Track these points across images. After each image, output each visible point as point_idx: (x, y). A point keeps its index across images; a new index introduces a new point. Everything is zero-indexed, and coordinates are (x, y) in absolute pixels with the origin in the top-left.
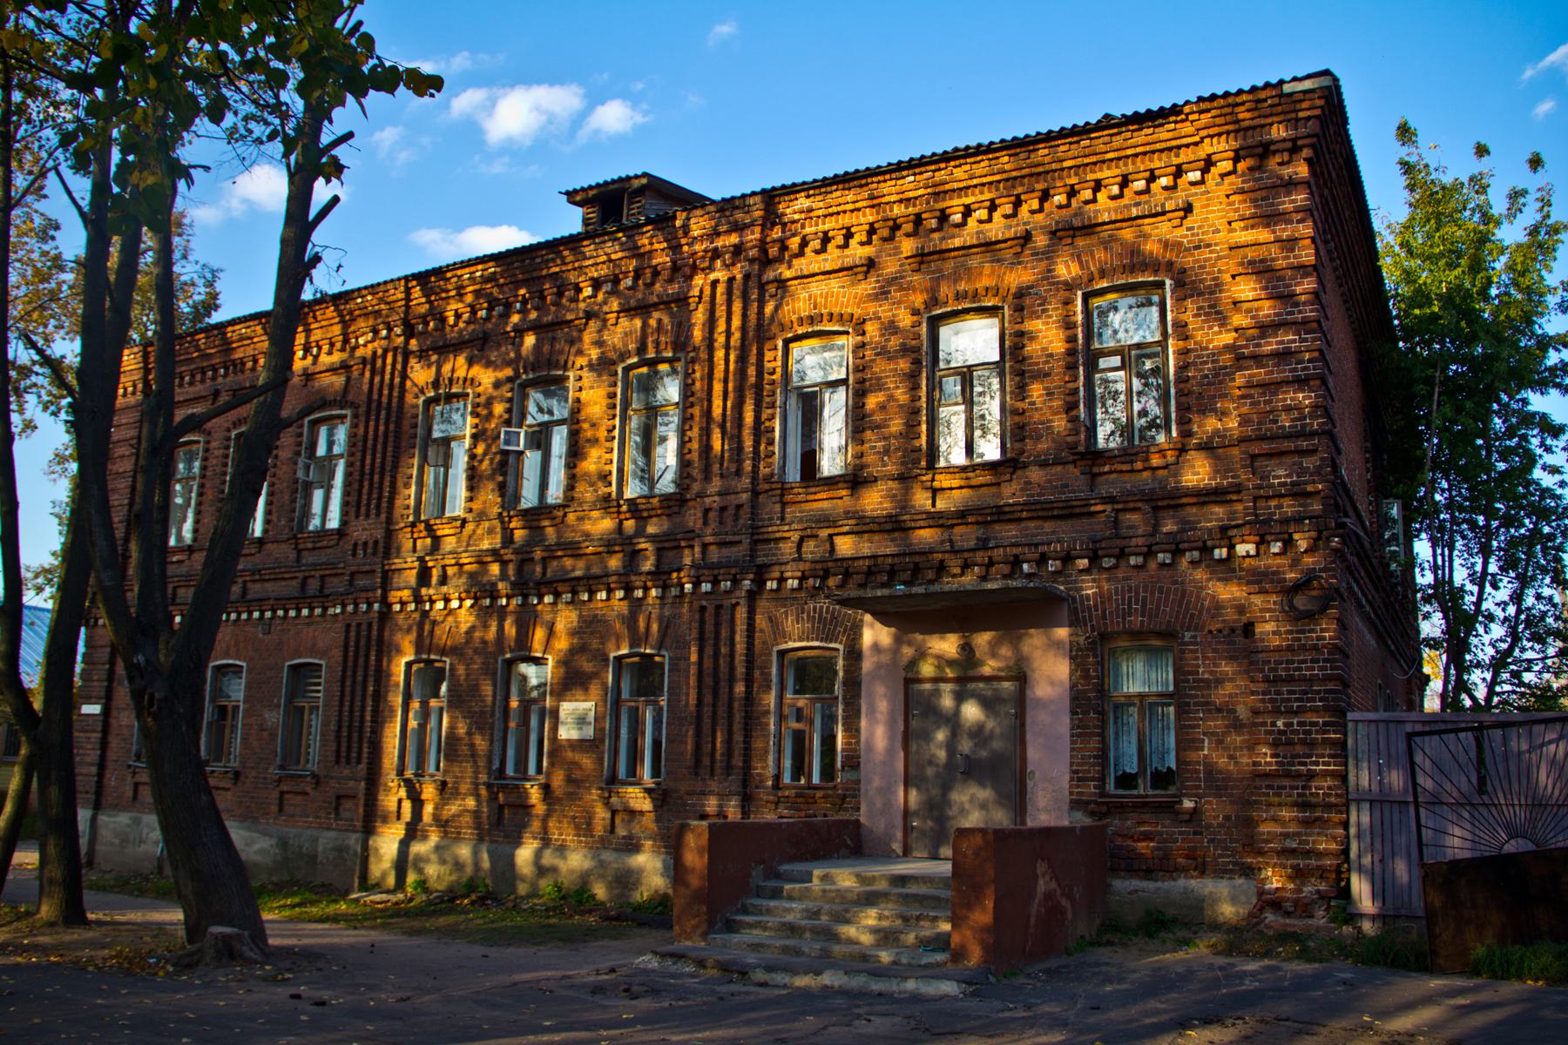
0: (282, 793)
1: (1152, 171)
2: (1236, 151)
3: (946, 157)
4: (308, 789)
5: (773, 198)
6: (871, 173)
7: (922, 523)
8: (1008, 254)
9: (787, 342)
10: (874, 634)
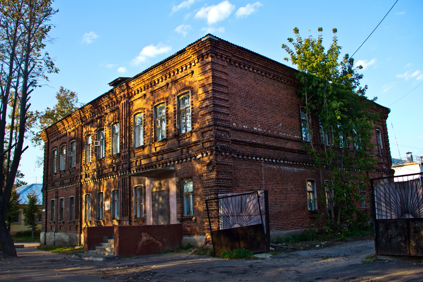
0: (70, 226)
1: (186, 64)
2: (197, 57)
5: (127, 83)
8: (165, 89)
9: (135, 116)
10: (147, 182)
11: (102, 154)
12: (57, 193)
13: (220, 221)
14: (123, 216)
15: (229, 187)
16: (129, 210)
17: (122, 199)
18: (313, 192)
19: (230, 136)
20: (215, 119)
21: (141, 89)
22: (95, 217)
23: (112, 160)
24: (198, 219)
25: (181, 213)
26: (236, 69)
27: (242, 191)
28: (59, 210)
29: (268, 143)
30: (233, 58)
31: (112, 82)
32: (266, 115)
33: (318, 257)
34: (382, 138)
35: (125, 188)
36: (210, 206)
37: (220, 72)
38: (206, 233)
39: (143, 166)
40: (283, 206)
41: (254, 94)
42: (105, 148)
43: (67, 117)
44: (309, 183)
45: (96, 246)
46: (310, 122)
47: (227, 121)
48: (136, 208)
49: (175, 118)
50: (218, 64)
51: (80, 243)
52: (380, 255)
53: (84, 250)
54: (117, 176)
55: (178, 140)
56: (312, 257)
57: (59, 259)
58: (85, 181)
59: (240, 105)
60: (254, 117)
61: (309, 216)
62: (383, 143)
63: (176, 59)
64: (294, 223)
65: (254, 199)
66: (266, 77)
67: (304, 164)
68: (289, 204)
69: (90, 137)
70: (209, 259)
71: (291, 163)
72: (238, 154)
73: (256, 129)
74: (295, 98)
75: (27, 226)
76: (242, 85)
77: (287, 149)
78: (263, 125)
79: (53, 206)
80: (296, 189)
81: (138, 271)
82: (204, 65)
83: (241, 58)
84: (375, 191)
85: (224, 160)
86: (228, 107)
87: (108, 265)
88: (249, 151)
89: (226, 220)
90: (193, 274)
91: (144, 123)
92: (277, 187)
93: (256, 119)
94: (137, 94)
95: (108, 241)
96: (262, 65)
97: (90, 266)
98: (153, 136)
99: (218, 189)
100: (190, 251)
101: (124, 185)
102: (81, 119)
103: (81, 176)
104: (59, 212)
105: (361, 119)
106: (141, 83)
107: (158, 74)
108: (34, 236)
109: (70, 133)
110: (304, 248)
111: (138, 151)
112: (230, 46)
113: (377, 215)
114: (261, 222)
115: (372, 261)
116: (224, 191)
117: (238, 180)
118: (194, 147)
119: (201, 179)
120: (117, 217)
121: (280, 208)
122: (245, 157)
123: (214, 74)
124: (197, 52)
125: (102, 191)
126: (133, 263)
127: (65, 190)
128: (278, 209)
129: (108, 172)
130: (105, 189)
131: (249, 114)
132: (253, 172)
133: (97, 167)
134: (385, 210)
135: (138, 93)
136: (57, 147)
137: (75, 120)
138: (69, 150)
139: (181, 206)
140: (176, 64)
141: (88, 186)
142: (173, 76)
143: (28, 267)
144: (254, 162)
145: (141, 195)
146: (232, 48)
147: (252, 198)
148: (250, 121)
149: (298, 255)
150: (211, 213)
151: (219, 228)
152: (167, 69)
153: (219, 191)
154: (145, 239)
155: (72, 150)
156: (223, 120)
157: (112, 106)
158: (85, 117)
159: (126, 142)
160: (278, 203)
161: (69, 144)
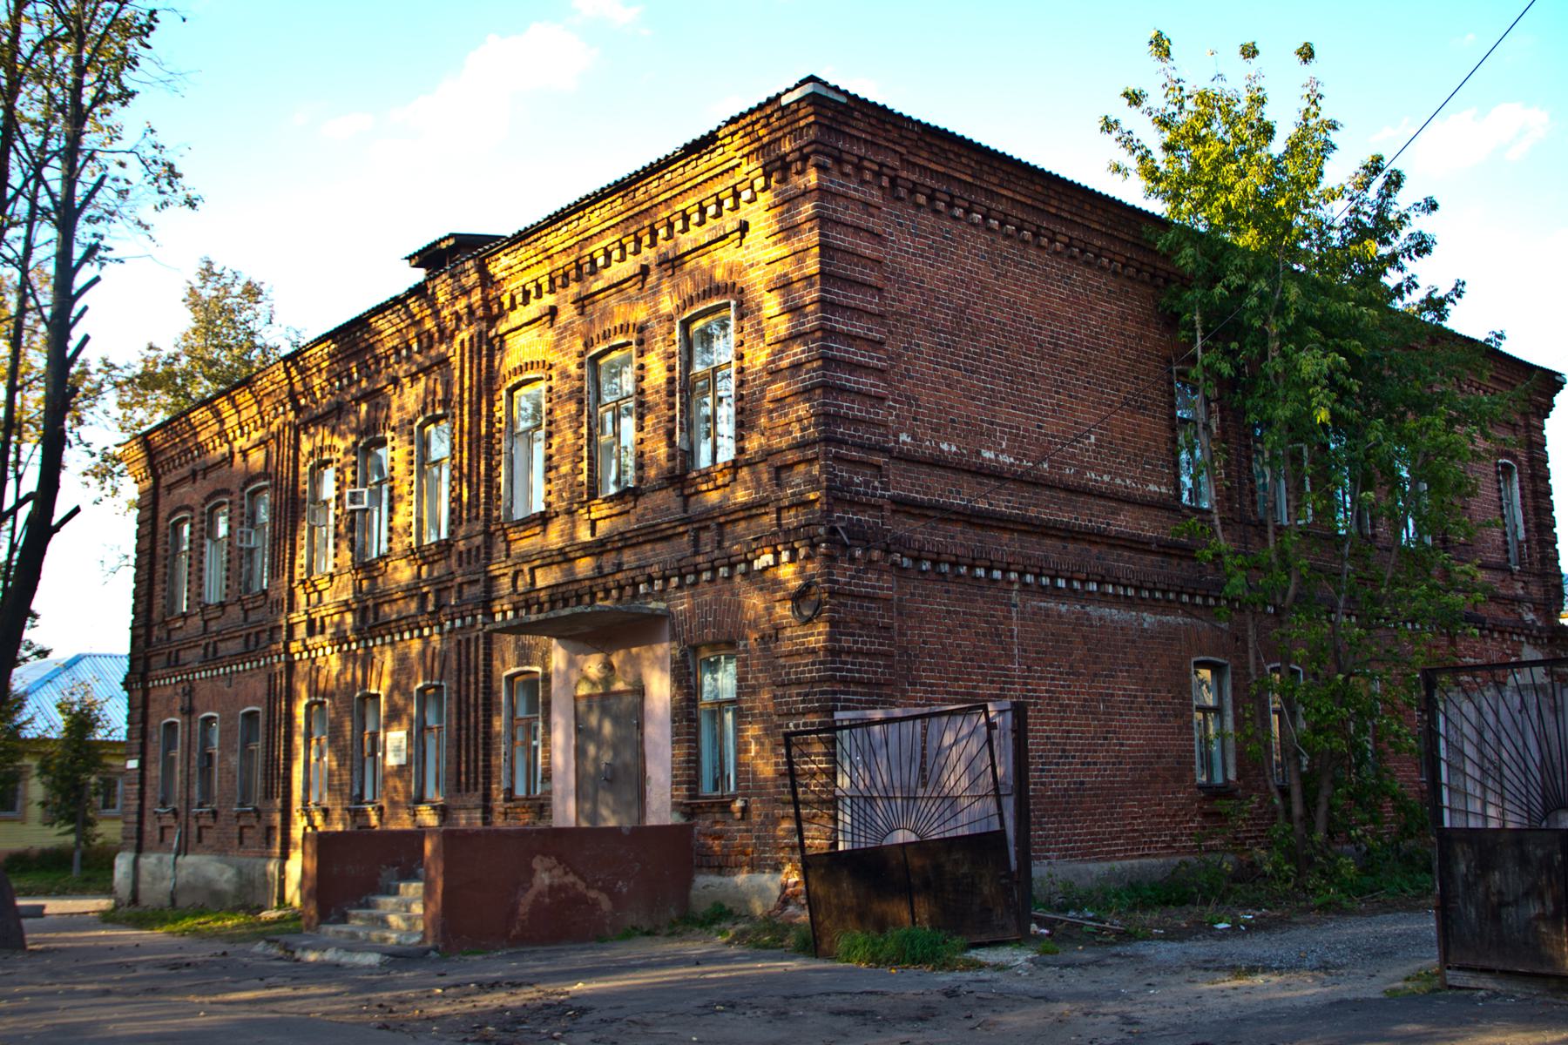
0: (242, 828)
1: (717, 194)
3: (579, 207)
4: (255, 824)
5: (484, 259)
6: (537, 229)
7: (578, 554)
8: (633, 291)
9: (511, 392)
10: (558, 657)
11: (378, 544)
12: (190, 693)
13: (840, 816)
14: (459, 791)
15: (878, 684)
16: (484, 766)
17: (454, 722)
18: (1218, 710)
19: (888, 483)
20: (826, 418)
21: (539, 287)
22: (348, 791)
23: (419, 568)
24: (756, 806)
25: (689, 783)
26: (916, 216)
27: (928, 699)
29: (1039, 513)
30: (904, 174)
31: (415, 254)
32: (1032, 400)
33: (1217, 969)
34: (1522, 497)
36: (800, 756)
37: (851, 230)
38: (783, 865)
39: (542, 594)
40: (1095, 764)
41: (985, 319)
42: (391, 519)
43: (237, 382)
44: (1206, 674)
45: (352, 908)
46: (1215, 430)
48: (512, 759)
49: (672, 407)
50: (846, 197)
51: (282, 897)
52: (1459, 969)
53: (303, 923)
54: (436, 629)
55: (682, 495)
56: (1193, 967)
57: (199, 957)
58: (306, 648)
60: (983, 408)
61: (1200, 808)
62: (1524, 515)
63: (681, 170)
64: (1137, 831)
65: (970, 735)
66: (1040, 247)
67: (1185, 598)
68: (1117, 757)
69: (330, 474)
70: (794, 965)
71: (1131, 592)
72: (916, 553)
73: (993, 456)
75: (55, 830)
77: (1114, 538)
78: (1017, 441)
79: (170, 744)
80: (1147, 697)
81: (518, 1004)
82: (788, 202)
83: (937, 172)
84: (1441, 719)
85: (860, 578)
86: (882, 371)
87: (400, 982)
88: (962, 545)
89: (862, 813)
90: (728, 1016)
91: (550, 423)
92: (1069, 686)
93: (994, 417)
94: (520, 307)
95: (397, 888)
96: (1023, 199)
97: (328, 984)
98: (584, 477)
99: (835, 692)
100: (722, 932)
101: (464, 668)
102: (293, 396)
103: (291, 628)
104: (195, 770)
105: (1428, 418)
106: (538, 263)
107: (608, 228)
108: (83, 868)
109: (245, 453)
110: (1166, 933)
111: (523, 534)
112: (894, 125)
113: (1446, 813)
114: (996, 827)
115: (1424, 987)
116: (859, 701)
117: (916, 656)
118: (743, 524)
119: (769, 649)
121: (1080, 770)
122: (945, 568)
123: (827, 236)
124: (763, 147)
125: (374, 691)
126: (499, 974)
127: (223, 684)
128: (1072, 777)
129: (399, 612)
130: (386, 682)
131: (965, 396)
132: (975, 627)
133: (354, 593)
134: (1478, 793)
135: (526, 302)
136: (189, 508)
137: (266, 402)
138: (242, 523)
139: (689, 754)
140: (680, 194)
141: (318, 670)
142: (666, 239)
144: (981, 588)
145: (532, 707)
147: (965, 731)
148: (967, 424)
149: (1141, 958)
150: (807, 786)
151: (835, 844)
152: (641, 212)
153: (839, 700)
154: (547, 881)
155: (253, 525)
156: (861, 421)
157: (419, 352)
158: (309, 391)
159: (474, 497)
160: (1076, 751)
161: (242, 498)
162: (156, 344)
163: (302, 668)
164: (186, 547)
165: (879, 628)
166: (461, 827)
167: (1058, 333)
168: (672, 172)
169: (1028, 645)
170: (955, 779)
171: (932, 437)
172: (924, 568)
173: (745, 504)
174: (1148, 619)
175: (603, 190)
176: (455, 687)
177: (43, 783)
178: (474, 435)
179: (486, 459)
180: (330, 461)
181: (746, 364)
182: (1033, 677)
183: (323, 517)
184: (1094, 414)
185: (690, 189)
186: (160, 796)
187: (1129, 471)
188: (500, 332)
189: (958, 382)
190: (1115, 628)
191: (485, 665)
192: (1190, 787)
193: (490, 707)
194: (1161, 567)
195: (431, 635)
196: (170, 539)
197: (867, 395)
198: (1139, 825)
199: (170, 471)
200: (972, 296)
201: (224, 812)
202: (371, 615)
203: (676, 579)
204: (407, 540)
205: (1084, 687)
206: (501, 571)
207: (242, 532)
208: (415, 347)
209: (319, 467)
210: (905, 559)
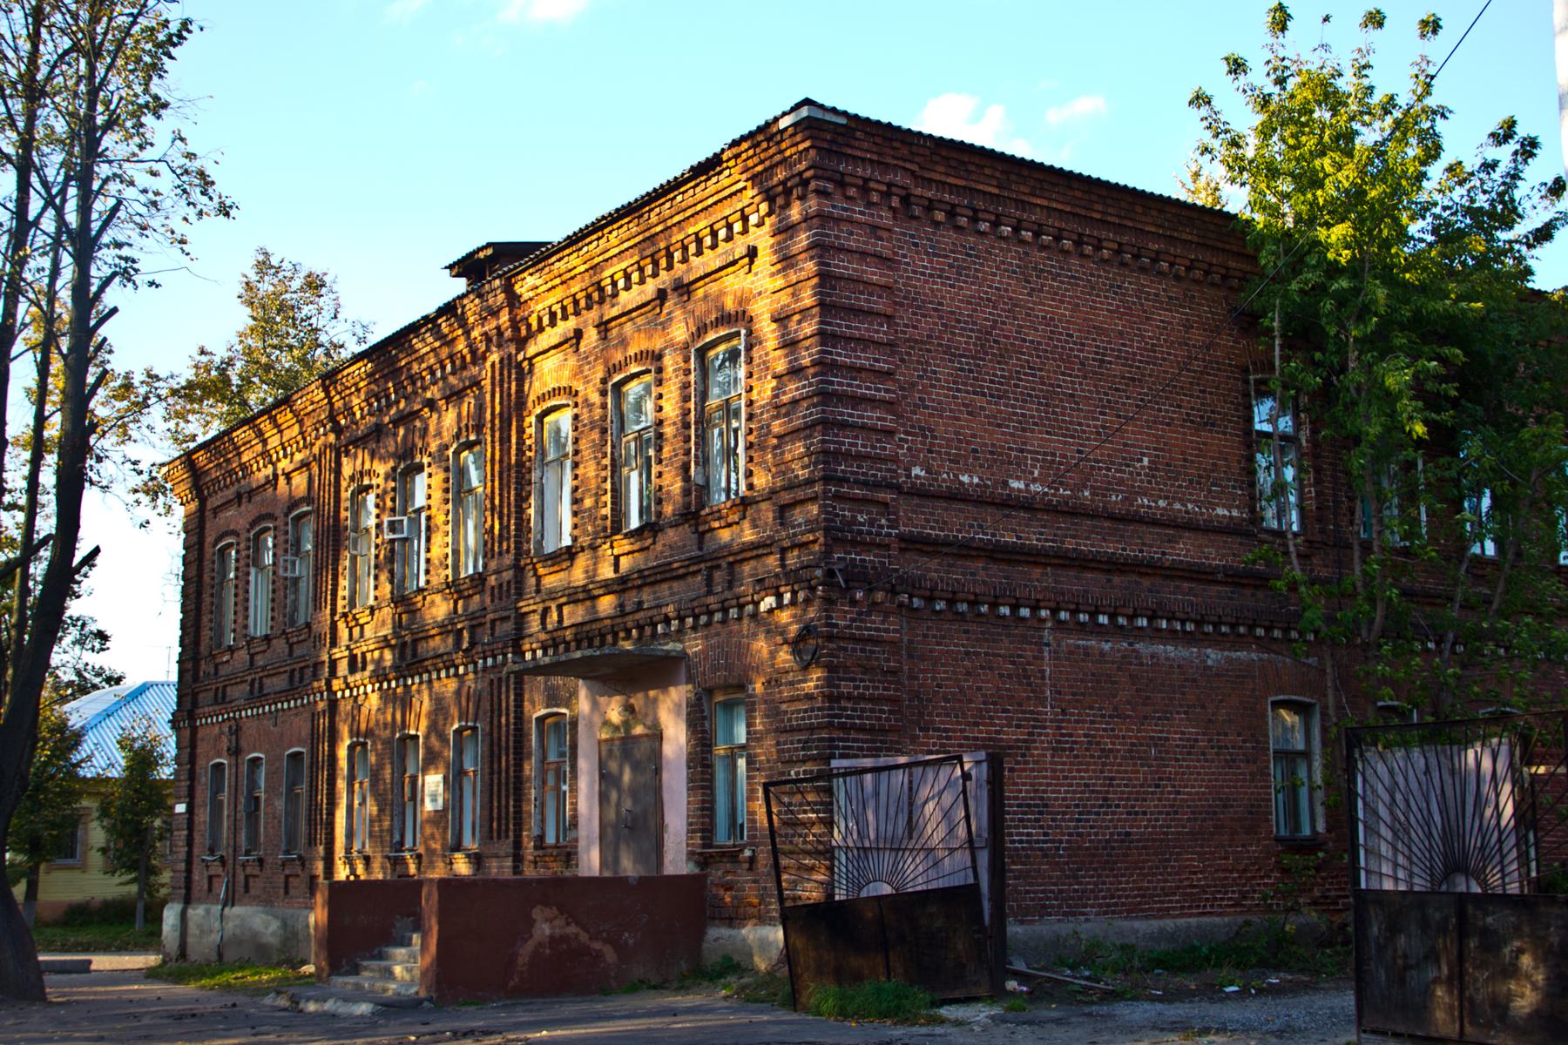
0: (287, 877)
1: (726, 218)
7: (601, 591)
9: (540, 418)
12: (236, 731)
15: (882, 731)
16: (515, 812)
19: (896, 521)
20: (826, 457)
25: (703, 831)
28: (241, 807)
30: (918, 191)
31: (455, 263)
32: (1071, 422)
35: (500, 721)
37: (857, 256)
40: (1145, 813)
41: (1015, 339)
42: (428, 550)
44: (1288, 717)
45: (364, 959)
46: (1304, 444)
47: (885, 460)
48: (543, 805)
50: (850, 221)
52: (1374, 1032)
54: (471, 667)
55: (696, 531)
58: (348, 686)
59: (950, 389)
60: (1011, 435)
66: (1083, 256)
67: (1260, 632)
71: (1190, 627)
72: (928, 593)
73: (1022, 486)
74: (1225, 341)
75: (117, 879)
76: (959, 301)
77: (1168, 568)
79: (217, 789)
80: (1210, 741)
82: (785, 230)
83: (956, 186)
86: (890, 403)
88: (984, 583)
93: (1024, 443)
94: (548, 329)
96: (1060, 206)
98: (607, 511)
99: (832, 740)
103: (333, 664)
104: (242, 815)
107: (627, 250)
109: (288, 476)
112: (903, 142)
114: (971, 881)
116: (861, 749)
117: (930, 700)
120: (471, 843)
121: (1126, 820)
122: (963, 607)
123: (828, 265)
125: (412, 732)
127: (268, 723)
130: (424, 724)
131: (990, 424)
133: (394, 628)
134: (1390, 855)
135: (553, 324)
137: (308, 422)
138: (286, 551)
139: (703, 801)
140: (692, 216)
143: (77, 1035)
146: (914, 149)
148: (992, 453)
149: (1111, 1017)
153: (837, 747)
154: (548, 932)
155: (297, 552)
156: (867, 457)
157: (453, 373)
158: (349, 410)
160: (1120, 799)
161: (287, 524)
162: (208, 348)
163: (345, 707)
164: (232, 575)
165: (885, 673)
166: (492, 876)
167: (1105, 349)
168: (683, 193)
169: (1063, 686)
170: (933, 830)
171: (951, 469)
172: (938, 608)
173: (752, 543)
174: (1212, 656)
175: (617, 210)
176: (488, 729)
177: (103, 827)
178: (505, 464)
179: (516, 489)
180: (371, 487)
181: (754, 395)
182: (1069, 721)
183: (365, 546)
184: (1148, 435)
185: (701, 211)
186: (207, 843)
187: (1190, 494)
188: (528, 356)
189: (982, 408)
190: (1171, 666)
191: (516, 706)
192: (1264, 839)
193: (520, 754)
194: (1231, 599)
195: (466, 673)
196: (216, 566)
197: (873, 429)
198: (1199, 880)
199: (215, 492)
200: (1001, 316)
201: (270, 860)
202: (409, 652)
203: (691, 620)
204: (443, 573)
205: (1132, 731)
206: (532, 608)
207: (286, 561)
208: (449, 368)
209: (360, 492)
210: (915, 600)
